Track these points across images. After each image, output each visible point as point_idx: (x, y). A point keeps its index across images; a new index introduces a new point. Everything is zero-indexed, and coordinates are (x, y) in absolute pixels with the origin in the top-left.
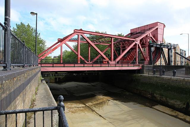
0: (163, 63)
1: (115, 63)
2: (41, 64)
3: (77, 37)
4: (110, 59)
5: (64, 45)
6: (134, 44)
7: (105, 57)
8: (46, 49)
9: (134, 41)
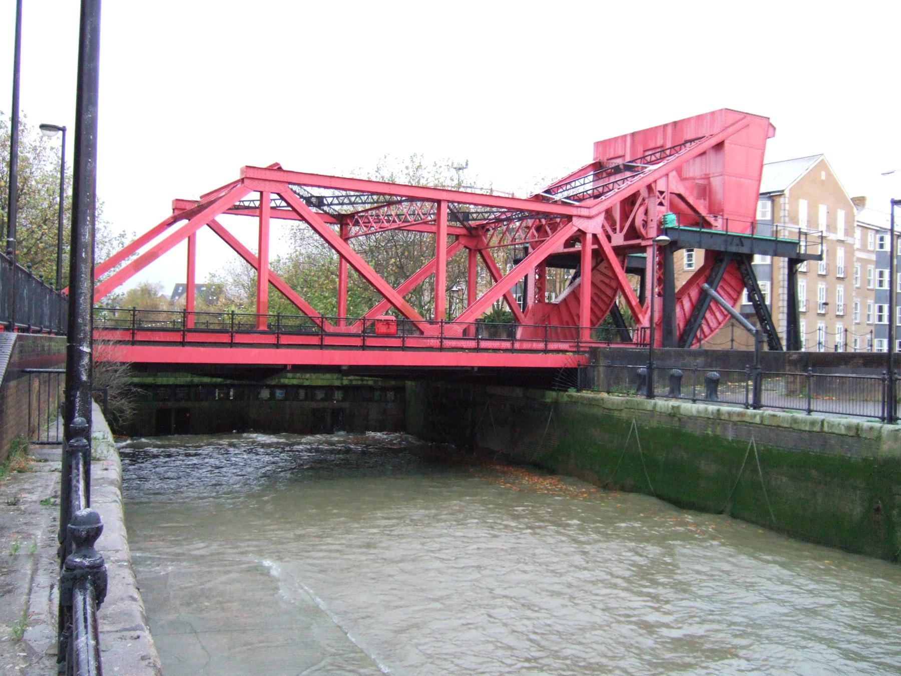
1: (437, 334)
3: (259, 198)
5: (204, 234)
6: (568, 231)
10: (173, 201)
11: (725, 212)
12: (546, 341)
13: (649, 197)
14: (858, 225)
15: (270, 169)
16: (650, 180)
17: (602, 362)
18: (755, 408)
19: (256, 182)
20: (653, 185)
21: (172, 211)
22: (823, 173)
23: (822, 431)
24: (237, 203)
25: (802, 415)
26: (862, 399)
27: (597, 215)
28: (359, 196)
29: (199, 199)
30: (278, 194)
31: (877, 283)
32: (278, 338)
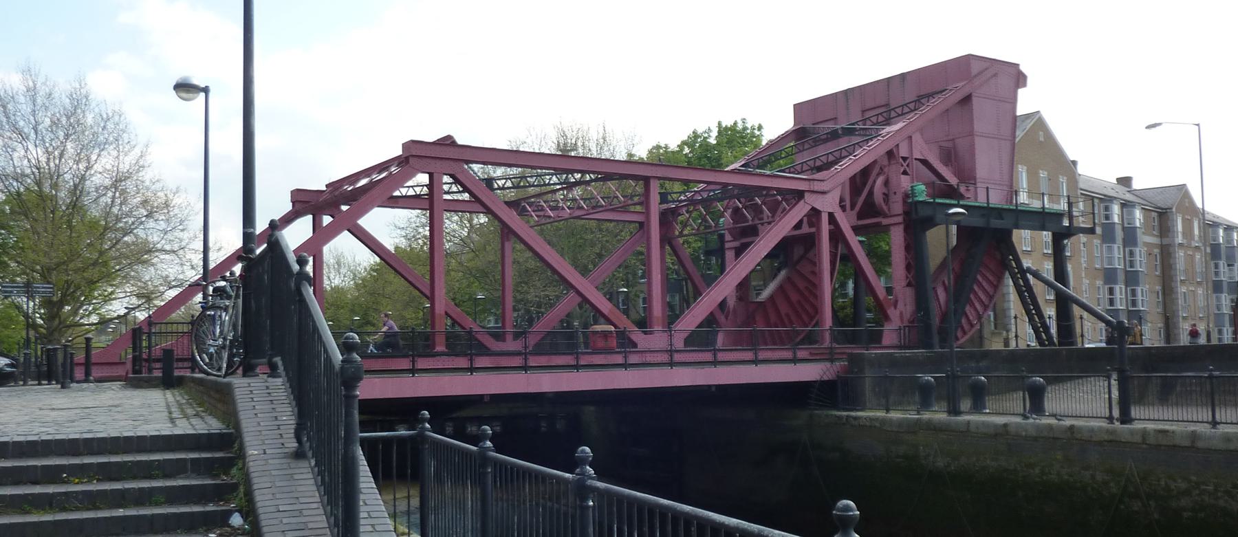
4: (643, 324)
6: (799, 212)
7: (605, 306)
9: (800, 195)
11: (978, 180)
12: (413, 356)
13: (889, 164)
14: (1082, 194)
17: (869, 373)
19: (425, 160)
27: (833, 189)
29: (325, 189)
30: (452, 176)
32: (413, 362)
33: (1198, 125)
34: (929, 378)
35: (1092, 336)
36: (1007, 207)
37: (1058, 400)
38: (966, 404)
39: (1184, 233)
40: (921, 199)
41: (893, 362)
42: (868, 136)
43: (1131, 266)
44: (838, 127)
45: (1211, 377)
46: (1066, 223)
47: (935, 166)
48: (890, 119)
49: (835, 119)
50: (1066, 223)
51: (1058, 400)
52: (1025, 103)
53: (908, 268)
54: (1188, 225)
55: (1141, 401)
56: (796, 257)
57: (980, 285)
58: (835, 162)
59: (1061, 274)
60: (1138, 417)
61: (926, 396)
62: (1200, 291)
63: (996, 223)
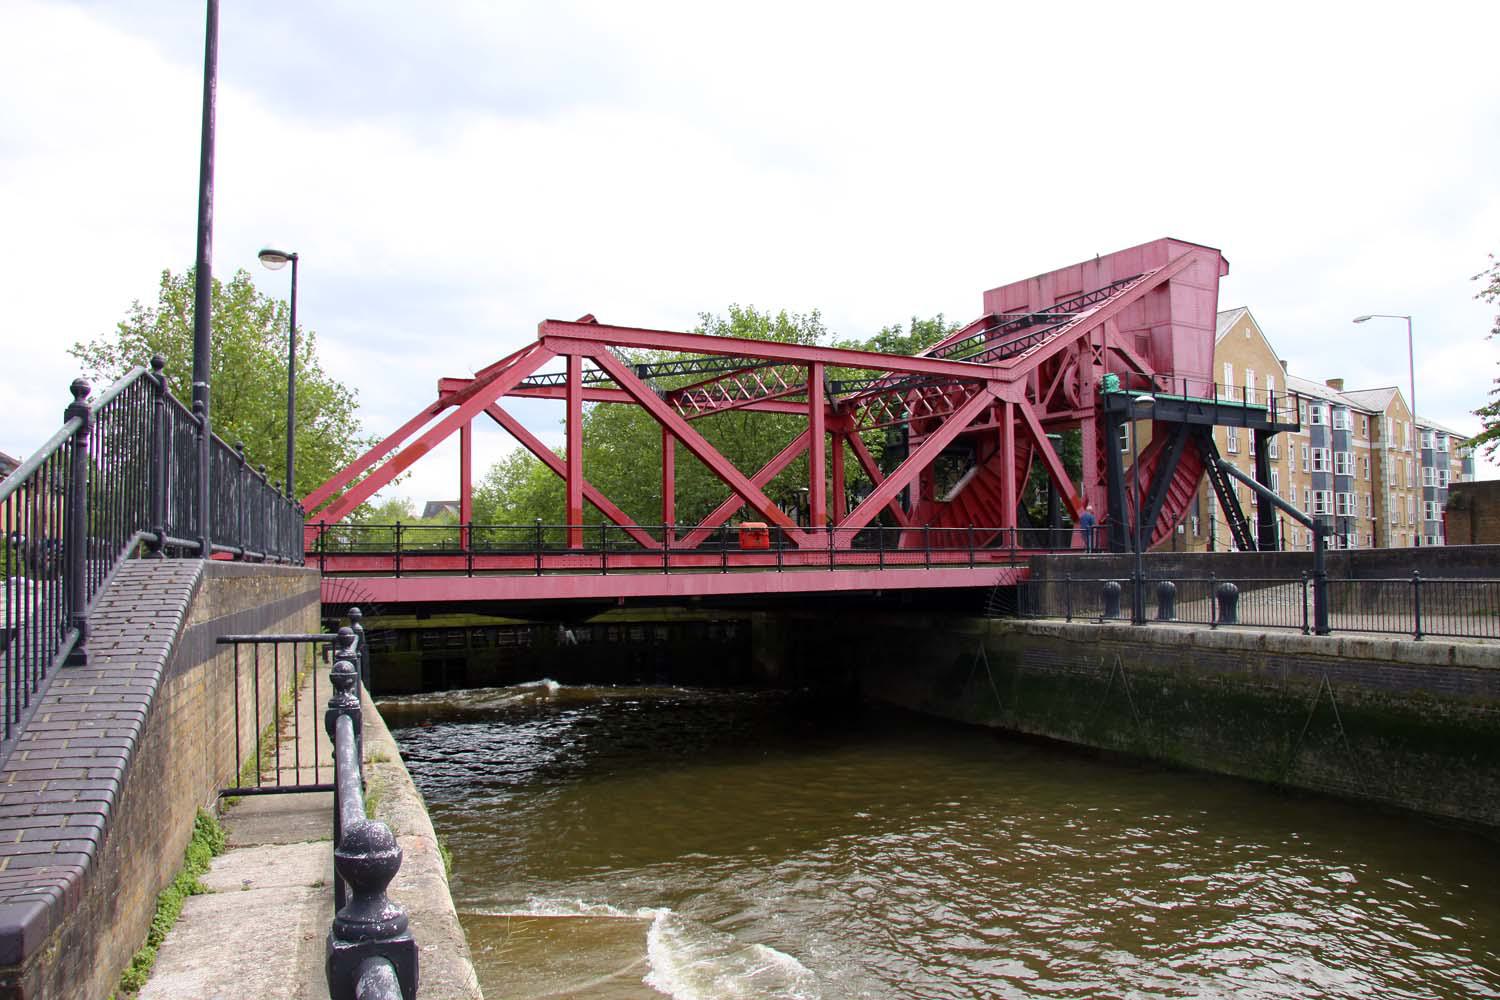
0: (1225, 541)
2: (321, 557)
3: (565, 371)
8: (361, 452)
9: (983, 383)
10: (440, 382)
11: (1176, 373)
15: (580, 324)
16: (1082, 332)
17: (1050, 576)
18: (1318, 633)
19: (561, 342)
20: (1086, 338)
21: (438, 394)
22: (1248, 331)
23: (1452, 664)
24: (525, 381)
25: (1408, 640)
26: (1380, 611)
28: (713, 360)
29: (474, 377)
31: (1313, 465)
32: (539, 560)
33: (1409, 318)
34: (1114, 583)
35: (1295, 539)
36: (1207, 401)
37: (1262, 607)
38: (1152, 612)
39: (1395, 438)
40: (1113, 391)
41: (1079, 566)
42: (1059, 321)
43: (1340, 471)
44: (1028, 314)
45: (1416, 583)
46: (1269, 420)
47: (1135, 361)
48: (1083, 306)
49: (1026, 307)
50: (1269, 420)
51: (1262, 607)
52: (1231, 293)
53: (1100, 465)
54: (1399, 426)
55: (1341, 608)
56: (985, 456)
57: (1177, 485)
58: (1019, 352)
59: (1263, 474)
60: (1335, 627)
61: (1110, 604)
62: (1410, 497)
63: (1194, 418)
